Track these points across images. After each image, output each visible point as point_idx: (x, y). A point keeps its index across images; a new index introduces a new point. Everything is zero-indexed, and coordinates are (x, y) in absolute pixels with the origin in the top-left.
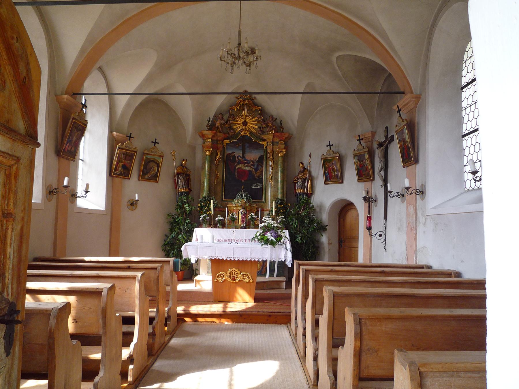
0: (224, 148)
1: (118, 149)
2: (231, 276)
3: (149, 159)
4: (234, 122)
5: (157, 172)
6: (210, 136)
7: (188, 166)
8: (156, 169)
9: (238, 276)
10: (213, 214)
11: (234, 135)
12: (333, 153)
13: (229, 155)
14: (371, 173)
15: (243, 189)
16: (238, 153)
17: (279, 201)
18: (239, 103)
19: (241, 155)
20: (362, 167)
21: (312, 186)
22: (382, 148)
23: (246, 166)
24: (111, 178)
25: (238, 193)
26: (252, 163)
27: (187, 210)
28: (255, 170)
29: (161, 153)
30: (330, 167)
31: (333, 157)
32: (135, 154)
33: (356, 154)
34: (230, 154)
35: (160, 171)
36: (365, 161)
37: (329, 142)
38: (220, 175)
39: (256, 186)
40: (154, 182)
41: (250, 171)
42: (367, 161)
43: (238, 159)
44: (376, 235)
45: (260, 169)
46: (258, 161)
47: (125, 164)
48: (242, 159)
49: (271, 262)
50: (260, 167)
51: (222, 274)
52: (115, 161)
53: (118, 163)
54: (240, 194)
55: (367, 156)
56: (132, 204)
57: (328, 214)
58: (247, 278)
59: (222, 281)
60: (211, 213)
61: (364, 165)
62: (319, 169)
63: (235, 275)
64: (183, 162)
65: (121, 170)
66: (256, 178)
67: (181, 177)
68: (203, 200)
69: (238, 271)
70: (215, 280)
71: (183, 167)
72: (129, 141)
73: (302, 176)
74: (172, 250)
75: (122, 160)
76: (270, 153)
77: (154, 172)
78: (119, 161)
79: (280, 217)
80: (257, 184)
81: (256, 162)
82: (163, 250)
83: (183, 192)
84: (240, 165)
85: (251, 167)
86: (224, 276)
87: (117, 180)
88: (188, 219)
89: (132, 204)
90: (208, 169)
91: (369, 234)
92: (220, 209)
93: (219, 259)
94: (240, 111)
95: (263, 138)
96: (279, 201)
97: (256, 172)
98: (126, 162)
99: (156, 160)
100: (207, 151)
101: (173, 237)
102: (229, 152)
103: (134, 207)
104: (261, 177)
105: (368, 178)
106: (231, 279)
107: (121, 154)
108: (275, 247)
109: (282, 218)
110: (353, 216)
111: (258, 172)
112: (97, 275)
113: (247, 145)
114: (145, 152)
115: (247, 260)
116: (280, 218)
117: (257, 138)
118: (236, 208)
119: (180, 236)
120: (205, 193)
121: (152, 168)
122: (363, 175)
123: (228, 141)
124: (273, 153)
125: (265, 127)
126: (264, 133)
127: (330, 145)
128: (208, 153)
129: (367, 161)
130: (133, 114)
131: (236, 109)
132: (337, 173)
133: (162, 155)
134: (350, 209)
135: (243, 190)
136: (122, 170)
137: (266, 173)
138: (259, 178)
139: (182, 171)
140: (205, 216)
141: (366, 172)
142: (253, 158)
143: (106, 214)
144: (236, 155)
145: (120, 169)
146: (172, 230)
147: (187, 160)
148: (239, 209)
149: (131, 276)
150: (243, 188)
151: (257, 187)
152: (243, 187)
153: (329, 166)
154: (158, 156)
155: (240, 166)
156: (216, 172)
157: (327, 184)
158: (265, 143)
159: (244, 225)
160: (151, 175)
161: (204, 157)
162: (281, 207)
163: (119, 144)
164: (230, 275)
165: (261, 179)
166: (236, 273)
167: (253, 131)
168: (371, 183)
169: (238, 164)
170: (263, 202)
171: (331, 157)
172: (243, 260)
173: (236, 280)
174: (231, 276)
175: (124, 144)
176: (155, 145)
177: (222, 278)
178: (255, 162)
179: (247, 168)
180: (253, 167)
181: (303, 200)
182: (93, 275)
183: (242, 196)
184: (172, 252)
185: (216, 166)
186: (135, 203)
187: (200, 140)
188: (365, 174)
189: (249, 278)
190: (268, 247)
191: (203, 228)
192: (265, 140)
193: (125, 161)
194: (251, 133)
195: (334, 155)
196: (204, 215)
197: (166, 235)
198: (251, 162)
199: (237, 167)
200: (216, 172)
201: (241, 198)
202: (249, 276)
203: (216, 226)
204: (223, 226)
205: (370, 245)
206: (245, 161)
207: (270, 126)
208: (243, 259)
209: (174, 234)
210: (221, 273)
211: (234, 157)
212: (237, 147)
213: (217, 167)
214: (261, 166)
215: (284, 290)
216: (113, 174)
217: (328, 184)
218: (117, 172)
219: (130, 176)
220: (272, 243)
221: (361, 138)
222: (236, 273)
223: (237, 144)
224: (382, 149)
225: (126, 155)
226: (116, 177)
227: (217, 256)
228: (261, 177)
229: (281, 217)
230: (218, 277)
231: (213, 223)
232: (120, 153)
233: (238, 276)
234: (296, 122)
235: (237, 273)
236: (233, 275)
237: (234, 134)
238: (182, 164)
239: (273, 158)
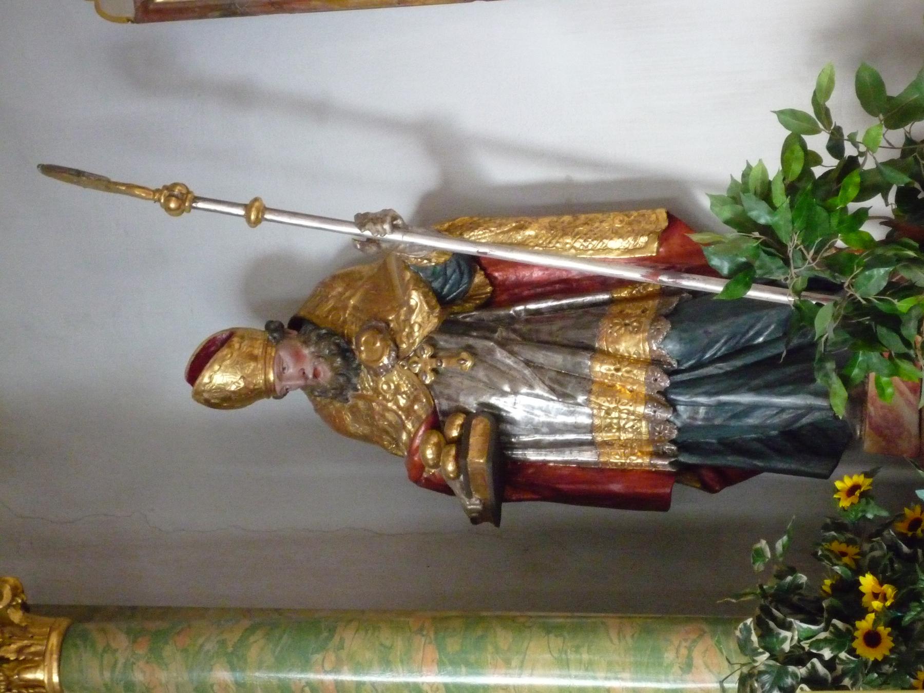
17: (798, 657)
96: (788, 639)
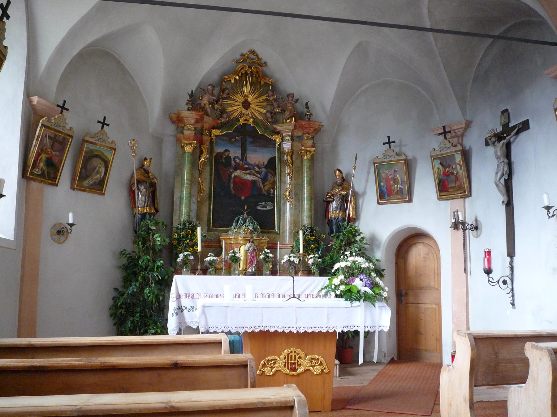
0: (211, 143)
1: (41, 128)
2: (288, 363)
3: (92, 151)
4: (229, 102)
5: (103, 176)
6: (193, 121)
7: (153, 170)
8: (103, 170)
9: (301, 361)
10: (200, 252)
11: (228, 122)
12: (396, 154)
13: (219, 155)
14: (466, 184)
15: (245, 211)
16: (235, 152)
18: (240, 70)
19: (240, 156)
20: (448, 175)
21: (355, 207)
22: (502, 142)
23: (248, 174)
24: (24, 182)
25: (236, 218)
26: (257, 169)
27: (156, 245)
28: (262, 180)
29: (112, 143)
30: (390, 177)
31: (396, 161)
32: (70, 140)
33: (438, 155)
34: (221, 154)
35: (109, 175)
36: (454, 166)
37: (389, 137)
38: (205, 187)
39: (264, 207)
40: (97, 193)
41: (254, 182)
42: (458, 166)
43: (235, 162)
44: (498, 281)
45: (270, 179)
46: (266, 167)
47: (51, 157)
48: (241, 162)
49: (367, 334)
50: (269, 176)
51: (272, 360)
52: (34, 150)
53: (38, 154)
54: (241, 218)
55: (458, 158)
56: (59, 233)
57: (384, 251)
58: (319, 365)
59: (271, 374)
60: (197, 250)
61: (452, 173)
62: (367, 181)
63: (296, 361)
64: (145, 163)
65: (44, 167)
66: (264, 194)
67: (142, 188)
68: (182, 226)
69: (302, 354)
70: (258, 372)
71: (145, 170)
72: (60, 115)
73: (339, 192)
74: (130, 316)
75: (46, 149)
76: (288, 153)
77: (98, 176)
78: (42, 150)
79: (312, 256)
80: (266, 204)
81: (264, 168)
82: (111, 316)
83: (146, 213)
84: (238, 171)
85: (256, 176)
86: (275, 363)
87: (35, 185)
88: (160, 260)
89: (59, 233)
90: (188, 175)
91: (489, 280)
92: (207, 244)
93: (268, 331)
94: (240, 84)
95: (275, 128)
97: (263, 183)
98: (54, 153)
99: (103, 154)
100: (187, 144)
101: (133, 291)
102: (219, 149)
103: (62, 238)
104: (272, 192)
105: (460, 193)
106: (288, 368)
107: (46, 136)
108: (374, 306)
109: (316, 257)
110: (420, 255)
111: (267, 183)
112: (166, 408)
113: (249, 140)
114: (86, 139)
115: (320, 332)
116: (311, 258)
117: (266, 129)
118: (235, 242)
119: (147, 291)
120: (184, 216)
121: (95, 168)
122: (450, 188)
123: (216, 132)
124: (293, 153)
125: (278, 113)
126: (276, 122)
127: (389, 143)
128: (188, 149)
129: (458, 166)
130: (66, 68)
131: (233, 81)
132: (401, 186)
133: (112, 146)
134: (415, 244)
135: (245, 213)
136: (45, 168)
137: (280, 186)
138: (269, 194)
139: (143, 178)
140: (188, 254)
141: (456, 183)
142: (259, 161)
143: (14, 249)
144: (232, 155)
145: (42, 165)
146: (127, 281)
147: (151, 159)
148: (240, 244)
149: (277, 403)
150: (246, 209)
151: (266, 208)
152: (246, 206)
153: (388, 174)
154: (107, 147)
155: (238, 173)
156: (200, 182)
157: (383, 204)
158: (278, 139)
159: (252, 270)
160: (93, 181)
161: (180, 157)
162: (311, 240)
163: (44, 119)
164: (286, 362)
165: (272, 195)
166: (297, 357)
167: (260, 117)
168: (463, 201)
169: (235, 169)
170: (276, 233)
171: (391, 161)
172: (313, 332)
173: (298, 369)
174: (288, 363)
175: (53, 119)
176: (102, 128)
177: (272, 368)
178: (263, 168)
179: (249, 177)
180: (259, 175)
181: (350, 227)
182: (154, 409)
183: (245, 222)
184: (131, 319)
185: (200, 172)
186: (65, 230)
187: (171, 129)
188: (453, 187)
189: (321, 364)
190: (359, 306)
191: (182, 276)
192: (278, 133)
193: (51, 152)
194: (255, 121)
195: (398, 158)
196: (186, 253)
197: (116, 289)
198: (255, 167)
199: (233, 176)
200: (200, 182)
201: (243, 225)
202: (321, 361)
203: (205, 272)
204: (217, 272)
205: (467, 300)
206: (246, 166)
207: (290, 109)
208: (314, 330)
209: (136, 286)
210: (269, 358)
211: (228, 158)
212: (233, 142)
213: (200, 173)
214: (273, 174)
215: (338, 379)
216: (28, 174)
217: (386, 203)
218: (37, 170)
219: (59, 180)
220: (367, 298)
221: (446, 130)
222: (297, 357)
223: (233, 138)
224: (503, 144)
225: (54, 139)
226: (34, 180)
227: (264, 326)
228: (272, 192)
229: (314, 256)
230: (264, 365)
231: (201, 266)
232: (44, 135)
233: (301, 361)
234: (328, 107)
235: (300, 358)
236: (291, 360)
237: (227, 121)
238: (143, 165)
239: (293, 161)
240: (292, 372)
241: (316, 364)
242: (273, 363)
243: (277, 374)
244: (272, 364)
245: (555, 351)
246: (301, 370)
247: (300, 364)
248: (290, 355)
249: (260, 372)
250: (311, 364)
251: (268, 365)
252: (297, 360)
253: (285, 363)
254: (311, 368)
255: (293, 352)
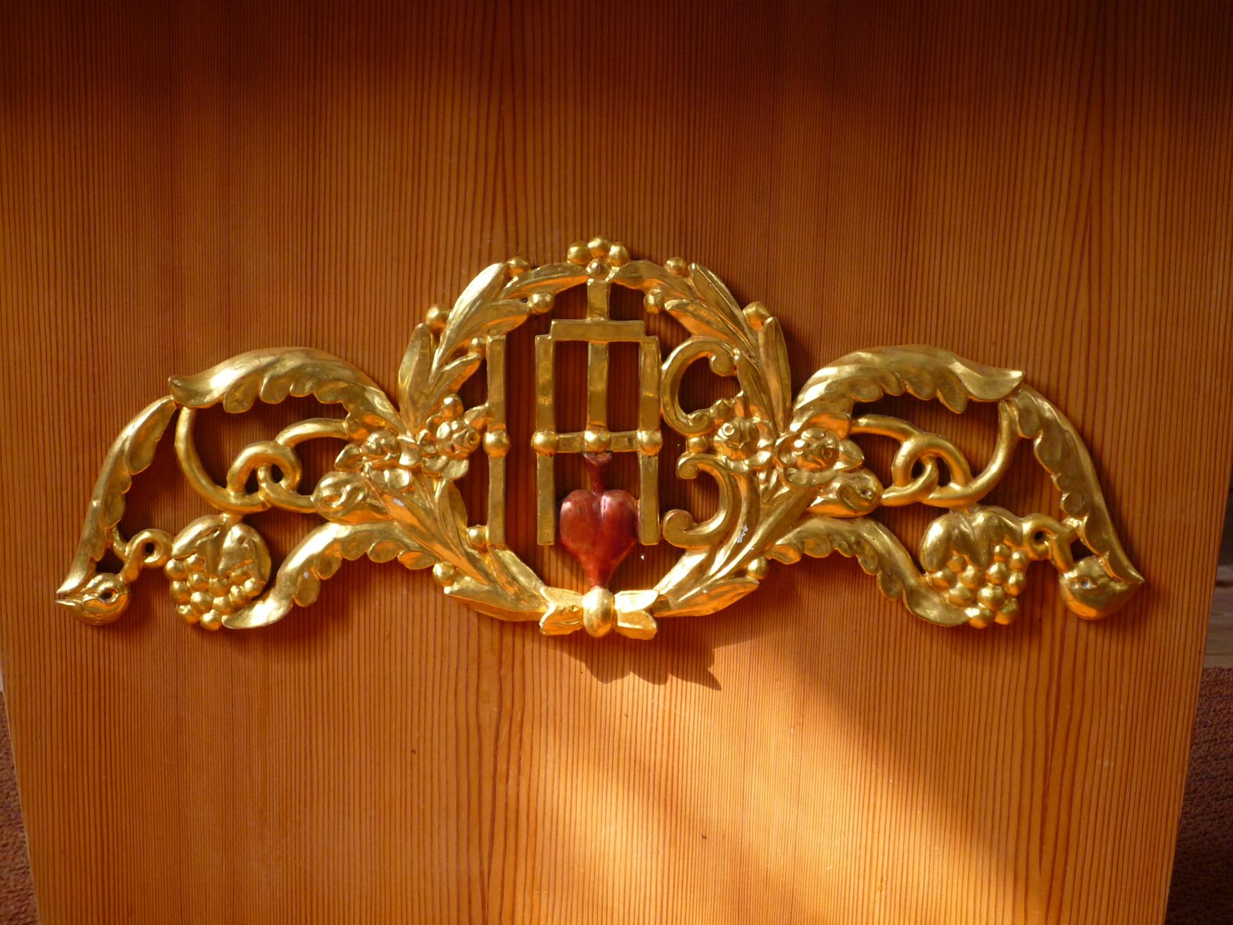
58: (987, 499)
59: (267, 612)
202: (1021, 451)
240: (460, 591)
241: (955, 487)
242: (288, 459)
243: (359, 616)
244: (276, 474)
245: (1070, 557)
246: (721, 565)
247: (706, 481)
248: (544, 344)
249: (102, 583)
250: (872, 482)
251: (219, 479)
252: (664, 427)
253: (478, 457)
254: (881, 539)
255: (598, 299)
